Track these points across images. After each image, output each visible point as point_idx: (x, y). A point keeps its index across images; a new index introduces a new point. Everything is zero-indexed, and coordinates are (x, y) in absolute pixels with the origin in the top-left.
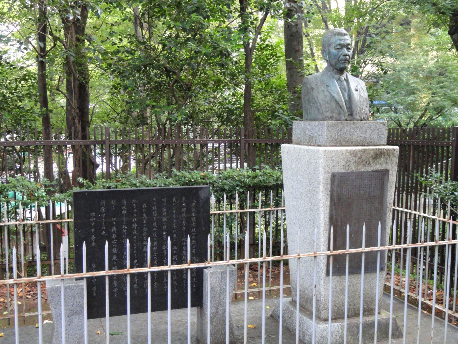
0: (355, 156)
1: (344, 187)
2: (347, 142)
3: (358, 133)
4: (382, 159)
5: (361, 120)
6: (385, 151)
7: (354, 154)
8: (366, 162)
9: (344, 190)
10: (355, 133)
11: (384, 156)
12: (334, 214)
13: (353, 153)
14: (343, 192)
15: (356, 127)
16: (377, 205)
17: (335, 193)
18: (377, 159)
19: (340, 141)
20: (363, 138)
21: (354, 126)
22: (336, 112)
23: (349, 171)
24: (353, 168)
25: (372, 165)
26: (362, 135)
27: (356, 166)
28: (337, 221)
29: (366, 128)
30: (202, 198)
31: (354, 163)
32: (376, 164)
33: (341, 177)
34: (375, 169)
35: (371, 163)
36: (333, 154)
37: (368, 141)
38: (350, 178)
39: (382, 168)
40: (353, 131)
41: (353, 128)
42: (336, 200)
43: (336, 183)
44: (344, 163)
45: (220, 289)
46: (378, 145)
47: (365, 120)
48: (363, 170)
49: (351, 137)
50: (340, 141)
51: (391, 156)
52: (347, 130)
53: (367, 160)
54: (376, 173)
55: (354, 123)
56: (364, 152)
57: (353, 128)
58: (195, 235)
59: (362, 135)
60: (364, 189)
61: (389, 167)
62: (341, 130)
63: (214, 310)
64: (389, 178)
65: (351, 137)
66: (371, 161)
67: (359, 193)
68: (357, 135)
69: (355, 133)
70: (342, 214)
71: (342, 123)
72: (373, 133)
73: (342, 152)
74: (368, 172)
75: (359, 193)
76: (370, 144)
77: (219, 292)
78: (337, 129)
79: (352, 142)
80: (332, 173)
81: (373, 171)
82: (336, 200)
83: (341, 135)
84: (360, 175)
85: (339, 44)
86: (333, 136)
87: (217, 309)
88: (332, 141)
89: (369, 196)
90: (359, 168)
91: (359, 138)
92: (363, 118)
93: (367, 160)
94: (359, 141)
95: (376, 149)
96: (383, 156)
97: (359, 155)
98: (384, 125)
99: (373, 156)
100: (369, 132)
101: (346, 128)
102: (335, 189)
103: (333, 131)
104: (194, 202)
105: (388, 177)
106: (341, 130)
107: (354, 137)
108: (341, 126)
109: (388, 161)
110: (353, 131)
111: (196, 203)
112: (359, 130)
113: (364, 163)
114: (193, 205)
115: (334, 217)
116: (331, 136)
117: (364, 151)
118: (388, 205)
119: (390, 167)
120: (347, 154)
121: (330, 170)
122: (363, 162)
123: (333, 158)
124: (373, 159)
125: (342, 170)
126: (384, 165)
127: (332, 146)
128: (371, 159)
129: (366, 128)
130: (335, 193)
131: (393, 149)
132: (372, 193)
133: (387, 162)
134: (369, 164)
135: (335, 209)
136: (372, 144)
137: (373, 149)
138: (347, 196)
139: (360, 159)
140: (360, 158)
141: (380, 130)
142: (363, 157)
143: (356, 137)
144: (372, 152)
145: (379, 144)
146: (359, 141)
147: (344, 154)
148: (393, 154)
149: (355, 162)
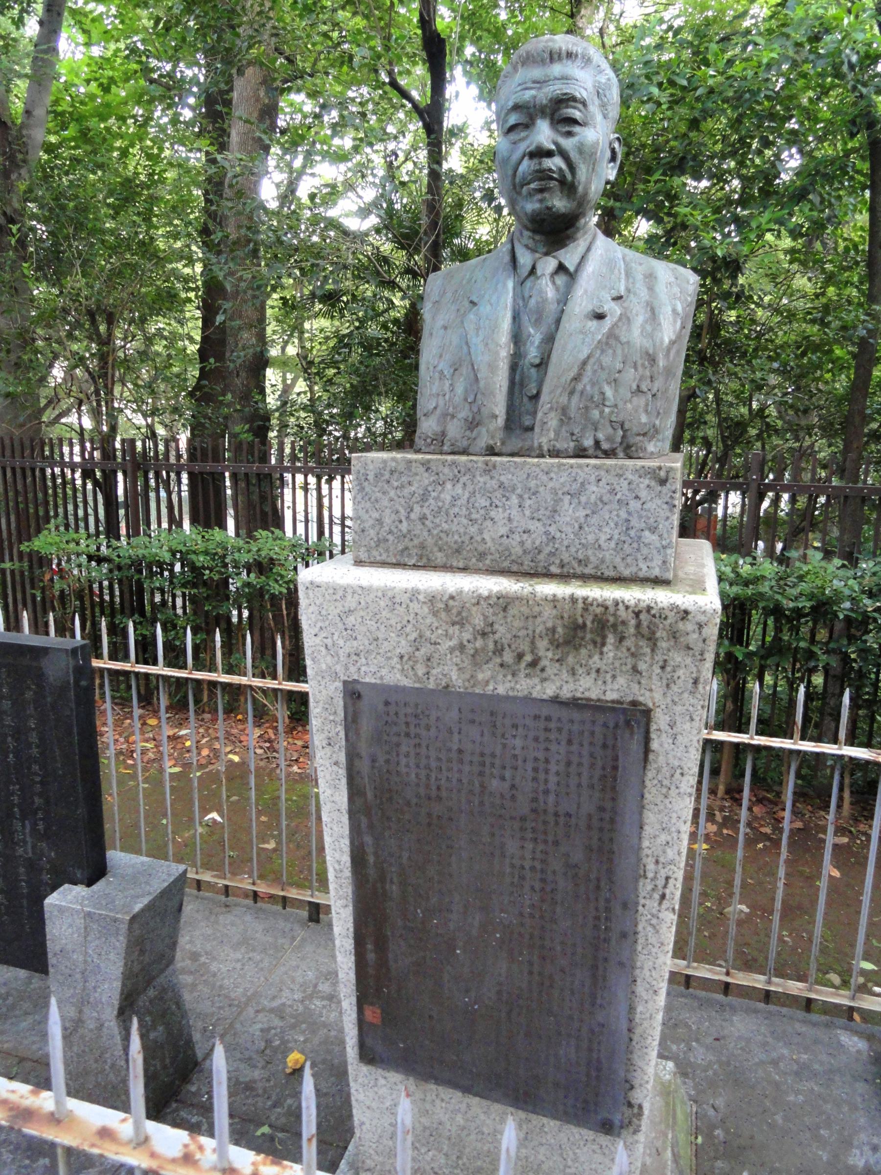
0: (461, 622)
1: (404, 749)
2: (458, 551)
3: (515, 512)
4: (609, 649)
5: (581, 453)
6: (622, 613)
7: (451, 609)
8: (520, 656)
9: (403, 761)
10: (498, 515)
11: (622, 639)
12: (370, 850)
13: (447, 609)
14: (403, 770)
15: (501, 485)
16: (578, 856)
17: (364, 766)
18: (577, 648)
19: (422, 546)
20: (538, 538)
21: (494, 483)
22: (462, 415)
23: (431, 686)
24: (452, 673)
25: (549, 671)
26: (533, 526)
27: (467, 663)
28: (382, 878)
29: (554, 491)
30: (51, 679)
31: (452, 650)
32: (573, 672)
33: (387, 703)
34: (566, 693)
35: (544, 662)
36: (351, 602)
37: (566, 557)
38: (434, 714)
39: (611, 696)
40: (483, 502)
41: (487, 493)
42: (370, 795)
43: (366, 725)
44: (404, 647)
45: (85, 962)
46: (619, 580)
47: (609, 454)
48: (501, 690)
49: (473, 530)
50: (422, 546)
51: (663, 644)
52: (455, 499)
53: (525, 646)
54: (576, 715)
55: (488, 470)
56: (505, 609)
57: (487, 493)
58: (41, 783)
59: (533, 526)
60: (508, 774)
61: (651, 695)
62: (424, 498)
63: (72, 1013)
64: (654, 745)
65: (473, 530)
66: (547, 655)
67: (483, 786)
68: (508, 523)
69: (498, 515)
70: (405, 855)
71: (427, 466)
72: (594, 520)
73: (391, 599)
74: (528, 700)
75: (483, 786)
76: (579, 570)
77: (81, 966)
78: (406, 491)
79: (482, 556)
80: (345, 683)
81: (555, 700)
82: (370, 795)
83: (423, 518)
84: (489, 712)
85: (516, 107)
86: (387, 520)
87: (80, 1012)
88: (380, 542)
89: (534, 811)
90: (480, 676)
91: (517, 537)
92: (588, 442)
93: (525, 646)
94: (518, 550)
95: (573, 600)
96: (611, 639)
97: (478, 621)
98: (663, 482)
99: (553, 630)
100: (570, 513)
101: (448, 492)
102: (364, 749)
103: (385, 502)
104: (29, 688)
105: (647, 740)
106: (424, 498)
107: (492, 534)
108: (426, 479)
109: (642, 666)
110: (483, 502)
111: (35, 693)
112: (515, 500)
113: (508, 657)
114: (29, 695)
115: (371, 859)
116: (380, 521)
117: (504, 603)
118: (651, 867)
119: (658, 696)
120: (414, 606)
121: (339, 668)
122: (499, 650)
123: (351, 620)
124: (556, 644)
125: (394, 677)
126: (621, 680)
127: (384, 564)
128: (542, 644)
129: (554, 491)
130: (364, 766)
131: (674, 607)
132: (551, 799)
133: (635, 670)
134: (533, 664)
135: (371, 826)
136: (588, 571)
137: (554, 601)
138: (422, 791)
139: (486, 632)
140: (484, 634)
141: (634, 505)
142: (501, 629)
143: (503, 531)
144: (548, 612)
145: (626, 573)
146: (518, 550)
147: (401, 610)
148: (674, 635)
149: (462, 647)
